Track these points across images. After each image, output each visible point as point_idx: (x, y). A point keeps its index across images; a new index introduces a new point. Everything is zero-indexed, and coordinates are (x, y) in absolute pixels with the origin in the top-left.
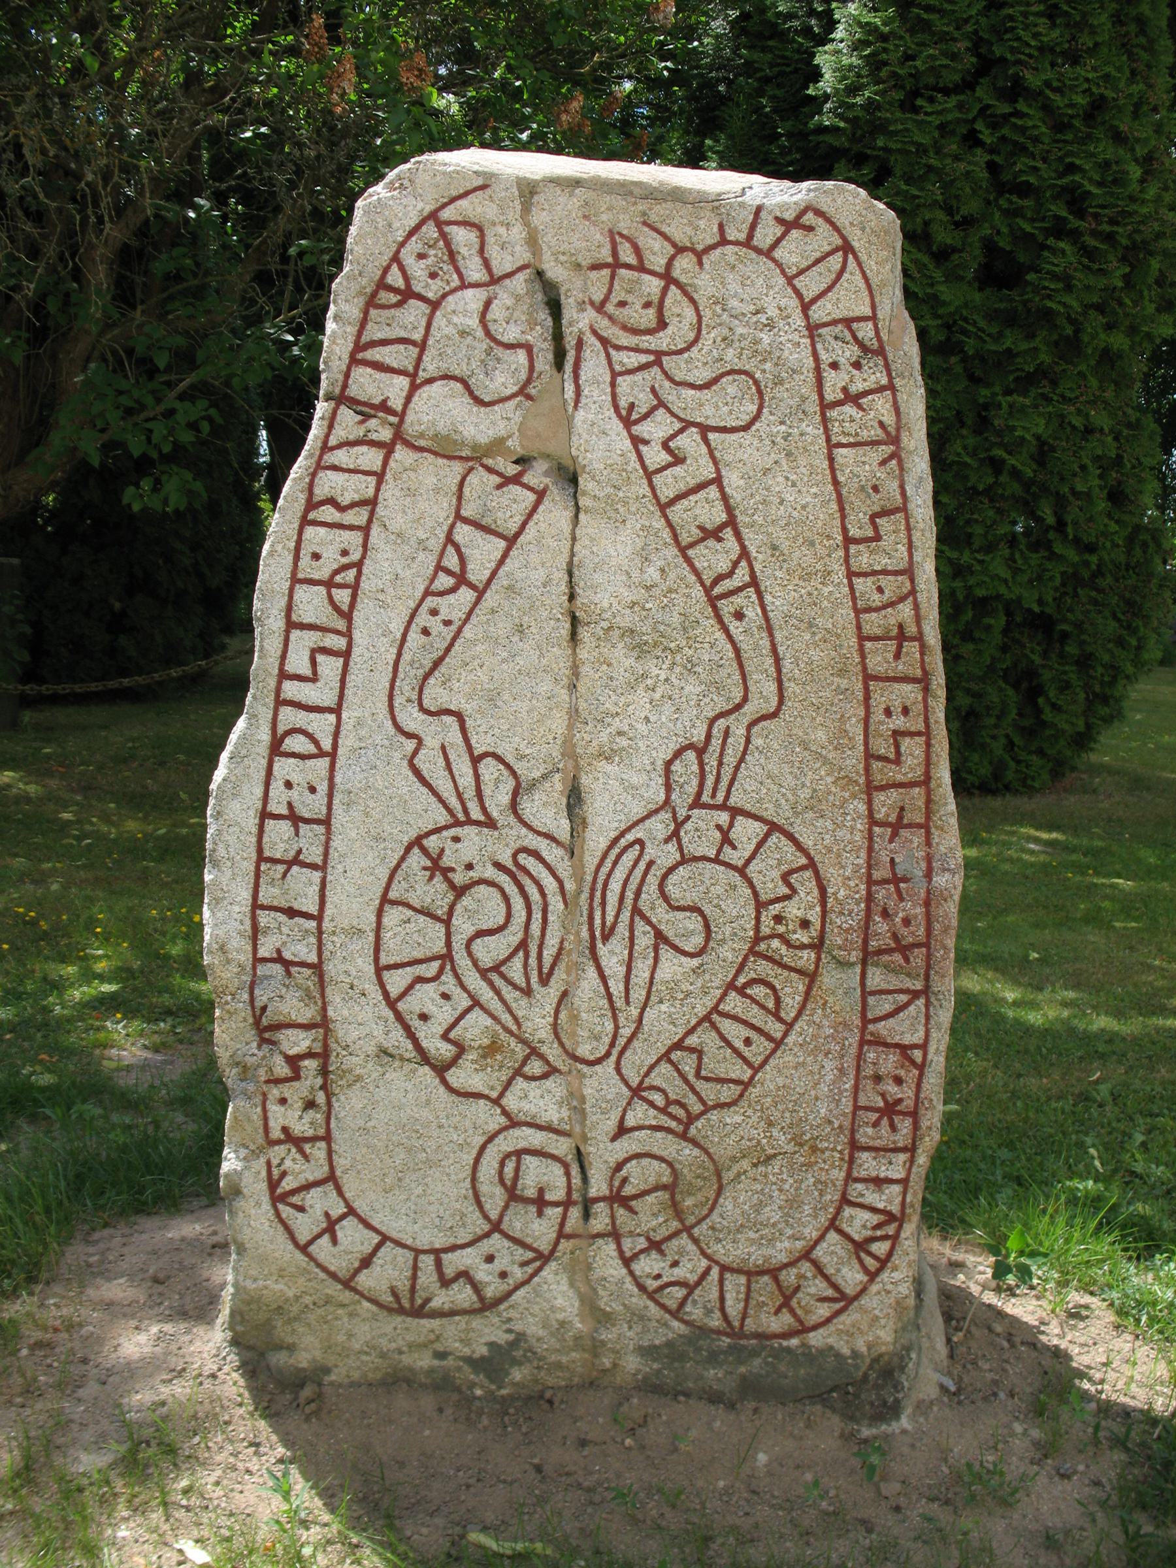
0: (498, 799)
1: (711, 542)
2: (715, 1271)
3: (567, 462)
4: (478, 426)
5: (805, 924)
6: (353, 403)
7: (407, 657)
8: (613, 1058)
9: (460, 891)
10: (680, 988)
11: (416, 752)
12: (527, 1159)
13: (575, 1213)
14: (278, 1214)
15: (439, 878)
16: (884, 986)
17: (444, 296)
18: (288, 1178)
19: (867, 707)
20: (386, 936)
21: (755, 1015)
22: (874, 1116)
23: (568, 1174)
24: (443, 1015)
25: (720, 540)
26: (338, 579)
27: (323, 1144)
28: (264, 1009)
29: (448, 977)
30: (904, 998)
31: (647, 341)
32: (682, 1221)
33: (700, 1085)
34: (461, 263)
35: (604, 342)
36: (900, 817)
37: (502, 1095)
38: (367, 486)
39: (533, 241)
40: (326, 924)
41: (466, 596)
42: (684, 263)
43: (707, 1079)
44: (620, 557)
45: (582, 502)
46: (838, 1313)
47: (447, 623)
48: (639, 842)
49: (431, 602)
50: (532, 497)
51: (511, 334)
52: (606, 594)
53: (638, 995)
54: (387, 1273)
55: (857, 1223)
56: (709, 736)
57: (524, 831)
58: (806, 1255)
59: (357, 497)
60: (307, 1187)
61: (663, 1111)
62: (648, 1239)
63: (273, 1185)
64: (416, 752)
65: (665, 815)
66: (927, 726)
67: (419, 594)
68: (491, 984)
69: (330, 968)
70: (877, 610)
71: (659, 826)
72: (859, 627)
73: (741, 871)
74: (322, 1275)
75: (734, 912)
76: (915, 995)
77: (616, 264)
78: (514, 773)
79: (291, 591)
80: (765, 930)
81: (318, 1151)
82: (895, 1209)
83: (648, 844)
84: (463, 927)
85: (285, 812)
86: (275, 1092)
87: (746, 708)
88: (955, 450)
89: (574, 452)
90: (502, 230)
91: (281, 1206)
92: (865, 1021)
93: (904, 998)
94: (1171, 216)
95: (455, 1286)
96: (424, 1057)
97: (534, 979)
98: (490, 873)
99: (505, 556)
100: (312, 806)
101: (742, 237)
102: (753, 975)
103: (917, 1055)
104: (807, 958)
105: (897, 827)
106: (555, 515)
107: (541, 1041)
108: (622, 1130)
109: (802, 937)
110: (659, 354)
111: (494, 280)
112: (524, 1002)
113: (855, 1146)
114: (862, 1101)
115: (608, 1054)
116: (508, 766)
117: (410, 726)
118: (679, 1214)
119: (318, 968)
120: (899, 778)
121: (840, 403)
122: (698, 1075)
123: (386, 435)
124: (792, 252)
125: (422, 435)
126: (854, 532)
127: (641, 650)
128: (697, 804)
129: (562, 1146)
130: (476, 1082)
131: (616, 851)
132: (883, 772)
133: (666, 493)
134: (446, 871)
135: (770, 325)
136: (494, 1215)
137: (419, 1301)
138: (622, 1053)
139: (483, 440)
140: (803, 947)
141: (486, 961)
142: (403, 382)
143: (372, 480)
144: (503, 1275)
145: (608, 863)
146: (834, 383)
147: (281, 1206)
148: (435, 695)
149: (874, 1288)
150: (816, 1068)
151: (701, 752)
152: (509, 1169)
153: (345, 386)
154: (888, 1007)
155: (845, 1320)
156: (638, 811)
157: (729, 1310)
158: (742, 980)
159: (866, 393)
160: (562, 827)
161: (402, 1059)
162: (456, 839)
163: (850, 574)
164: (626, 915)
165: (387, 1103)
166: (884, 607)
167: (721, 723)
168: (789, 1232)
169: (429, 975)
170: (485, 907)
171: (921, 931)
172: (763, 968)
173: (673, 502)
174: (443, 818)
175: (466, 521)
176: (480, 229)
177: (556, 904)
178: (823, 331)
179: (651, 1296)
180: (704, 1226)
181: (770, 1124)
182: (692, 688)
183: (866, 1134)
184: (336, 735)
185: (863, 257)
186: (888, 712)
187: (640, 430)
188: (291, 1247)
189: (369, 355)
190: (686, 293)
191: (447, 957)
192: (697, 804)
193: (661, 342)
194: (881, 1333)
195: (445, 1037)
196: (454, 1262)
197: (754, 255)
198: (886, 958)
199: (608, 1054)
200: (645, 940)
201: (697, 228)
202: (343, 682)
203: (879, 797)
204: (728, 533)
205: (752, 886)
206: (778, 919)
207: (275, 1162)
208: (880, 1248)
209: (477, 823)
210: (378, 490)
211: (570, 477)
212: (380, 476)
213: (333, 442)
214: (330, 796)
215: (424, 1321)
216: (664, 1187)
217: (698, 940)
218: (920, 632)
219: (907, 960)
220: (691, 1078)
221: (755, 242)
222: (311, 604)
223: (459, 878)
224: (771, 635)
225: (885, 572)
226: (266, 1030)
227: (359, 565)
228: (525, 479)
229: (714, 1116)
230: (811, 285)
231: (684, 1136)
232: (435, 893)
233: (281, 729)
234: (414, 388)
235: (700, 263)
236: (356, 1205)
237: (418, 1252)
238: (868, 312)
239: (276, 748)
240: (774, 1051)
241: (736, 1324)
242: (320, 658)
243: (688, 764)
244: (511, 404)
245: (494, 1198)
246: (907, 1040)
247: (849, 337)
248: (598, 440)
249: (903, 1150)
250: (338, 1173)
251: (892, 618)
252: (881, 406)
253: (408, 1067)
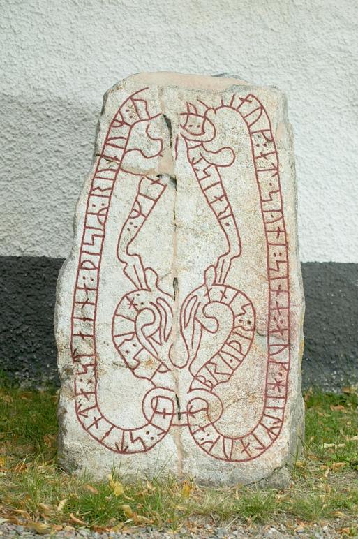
1: (218, 201)
2: (221, 438)
3: (174, 177)
4: (146, 165)
5: (249, 322)
6: (105, 157)
7: (123, 237)
8: (188, 366)
9: (139, 312)
10: (210, 344)
11: (126, 267)
12: (160, 399)
13: (176, 417)
14: (78, 417)
15: (132, 307)
16: (275, 343)
17: (134, 124)
18: (82, 406)
19: (268, 253)
20: (115, 326)
21: (233, 352)
22: (273, 386)
23: (173, 404)
24: (134, 351)
25: (221, 201)
26: (101, 213)
27: (94, 395)
28: (75, 350)
29: (135, 339)
30: (282, 347)
31: (199, 138)
32: (210, 421)
33: (216, 375)
34: (139, 113)
35: (185, 138)
36: (279, 289)
37: (152, 378)
38: (110, 184)
40: (97, 322)
41: (141, 218)
42: (211, 113)
43: (218, 373)
45: (178, 189)
46: (262, 453)
47: (135, 227)
48: (196, 296)
49: (131, 220)
50: (162, 187)
51: (156, 136)
52: (187, 218)
53: (196, 346)
54: (115, 438)
55: (268, 422)
56: (218, 263)
57: (160, 292)
59: (107, 187)
60: (88, 409)
61: (204, 383)
62: (199, 427)
63: (77, 409)
64: (126, 267)
65: (204, 288)
66: (287, 259)
67: (127, 218)
68: (149, 341)
69: (98, 337)
70: (271, 223)
71: (203, 291)
72: (265, 228)
73: (228, 306)
74: (93, 439)
75: (226, 320)
76: (285, 346)
77: (189, 113)
78: (156, 274)
79: (86, 216)
80: (236, 325)
81: (92, 397)
82: (281, 418)
83: (199, 297)
84: (140, 323)
85: (83, 287)
86: (79, 377)
87: (230, 254)
89: (175, 173)
90: (152, 102)
91: (79, 416)
92: (269, 355)
93: (282, 347)
95: (136, 442)
97: (163, 338)
98: (149, 305)
99: (154, 206)
101: (229, 104)
102: (233, 339)
103: (287, 366)
104: (250, 334)
105: (279, 291)
106: (169, 192)
107: (165, 360)
108: (191, 390)
109: (248, 327)
110: (202, 142)
111: (150, 118)
112: (159, 347)
113: (267, 396)
114: (269, 382)
115: (186, 365)
116: (155, 272)
117: (124, 260)
118: (210, 419)
119: (94, 337)
120: (279, 276)
121: (259, 157)
122: (215, 372)
123: (116, 167)
124: (245, 109)
125: (127, 167)
126: (264, 198)
127: (196, 235)
128: (214, 284)
129: (172, 395)
130: (144, 374)
131: (188, 299)
132: (274, 274)
133: (204, 186)
134: (135, 305)
135: (237, 133)
136: (149, 418)
137: (124, 448)
138: (190, 365)
139: (147, 169)
140: (249, 330)
141: (148, 334)
142: (122, 151)
143: (112, 182)
144: (152, 438)
145: (186, 303)
147: (79, 416)
148: (132, 249)
149: (274, 445)
150: (253, 370)
151: (216, 268)
152: (155, 401)
153: (103, 439)
154: (276, 350)
155: (265, 455)
156: (195, 286)
157: (226, 451)
158: (229, 341)
159: (267, 154)
160: (172, 291)
161: (120, 366)
162: (138, 295)
163: (263, 211)
164: (192, 320)
165: (115, 380)
166: (273, 222)
167: (222, 259)
168: (246, 425)
169: (129, 338)
170: (147, 316)
171: (287, 325)
172: (235, 337)
173: (206, 189)
174: (134, 288)
175: (141, 194)
176: (146, 102)
177: (169, 315)
178: (254, 134)
180: (218, 422)
181: (239, 388)
182: (213, 247)
183: (270, 393)
184: (100, 262)
185: (269, 113)
186: (275, 255)
187: (196, 166)
188: (82, 429)
189: (111, 142)
190: (211, 123)
191: (135, 333)
192: (214, 284)
193: (203, 138)
194: (277, 460)
195: (134, 358)
196: (136, 434)
197: (232, 110)
198: (275, 333)
199: (186, 365)
200: (198, 326)
201: (214, 102)
202: (102, 245)
203: (272, 282)
204: (224, 199)
205: (232, 310)
206: (240, 321)
207: (78, 401)
208: (276, 431)
209: (145, 290)
210: (113, 185)
211: (175, 181)
212: (114, 180)
213: (99, 169)
214: (98, 281)
215: (125, 455)
216: (204, 409)
217: (215, 328)
218: (285, 229)
219: (282, 334)
220: (213, 373)
221: (233, 106)
222: (92, 221)
223: (139, 307)
224: (237, 231)
225: (273, 211)
226: (76, 357)
227: (107, 209)
228: (160, 182)
229: (220, 385)
230: (250, 120)
231: (211, 392)
232: (131, 312)
233: (82, 260)
234: (125, 152)
235: (215, 113)
236: (104, 415)
237: (124, 430)
238: (269, 128)
239: (81, 266)
240: (240, 364)
241: (229, 456)
242: (95, 238)
243: (211, 273)
244: (157, 157)
245: (149, 412)
246: (283, 361)
247: (262, 136)
248: (183, 170)
249: (283, 398)
250: (99, 404)
251: (276, 225)
252: (273, 158)
253: (122, 368)
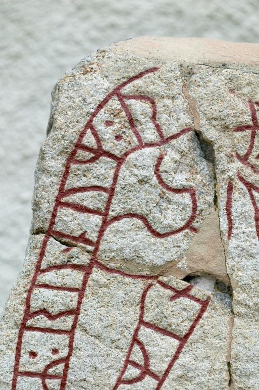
4: (156, 252)
39: (192, 110)
51: (179, 179)
123: (85, 259)
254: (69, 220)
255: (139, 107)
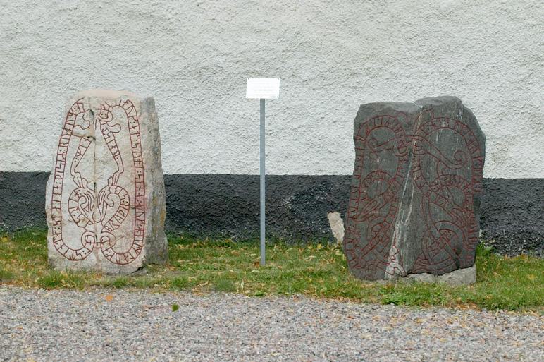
0: (85, 184)
4: (82, 132)
9: (80, 198)
10: (111, 211)
21: (121, 216)
24: (77, 215)
39: (90, 106)
42: (111, 108)
44: (101, 150)
51: (87, 119)
52: (99, 156)
54: (69, 254)
58: (128, 251)
71: (107, 188)
75: (117, 200)
84: (80, 202)
88: (538, 183)
94: (543, 17)
96: (75, 221)
100: (60, 186)
108: (102, 232)
123: (70, 134)
124: (126, 107)
129: (93, 234)
130: (82, 225)
146: (131, 125)
165: (70, 228)
170: (83, 200)
179: (106, 257)
196: (78, 252)
200: (105, 204)
230: (128, 111)
232: (76, 198)
245: (84, 242)
248: (98, 135)
251: (138, 159)
254: (67, 126)
255: (80, 105)
